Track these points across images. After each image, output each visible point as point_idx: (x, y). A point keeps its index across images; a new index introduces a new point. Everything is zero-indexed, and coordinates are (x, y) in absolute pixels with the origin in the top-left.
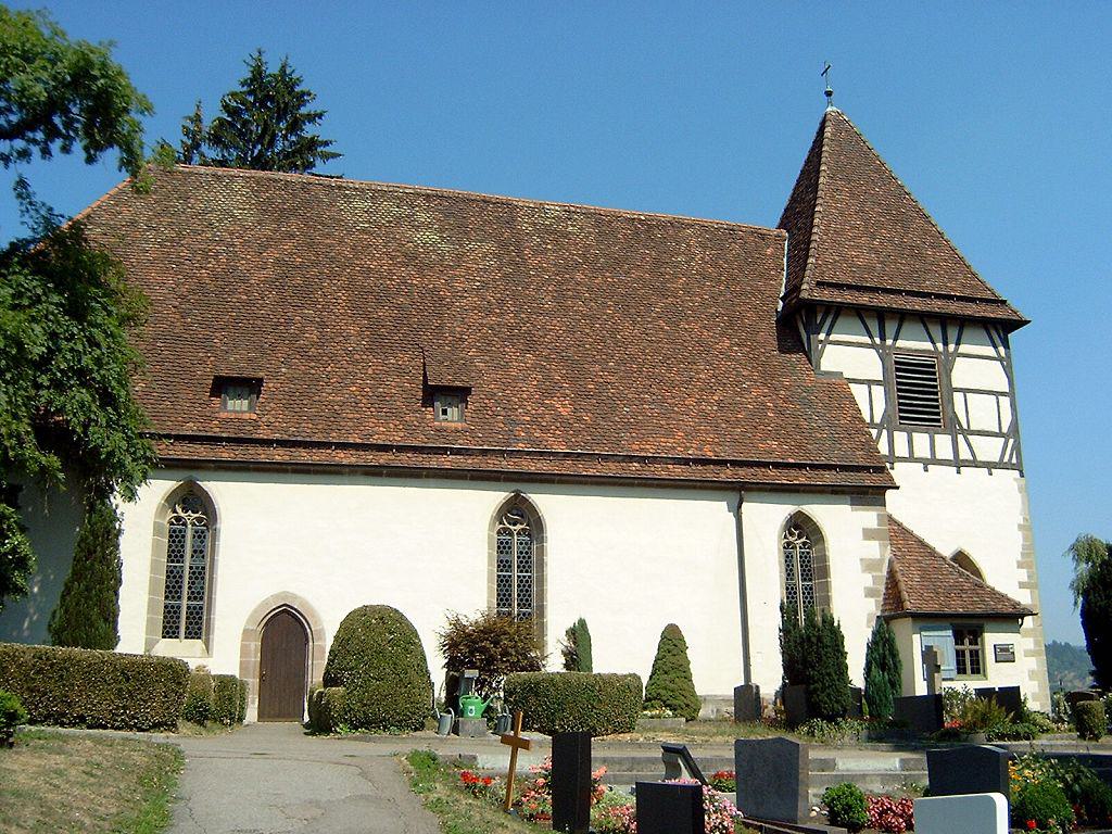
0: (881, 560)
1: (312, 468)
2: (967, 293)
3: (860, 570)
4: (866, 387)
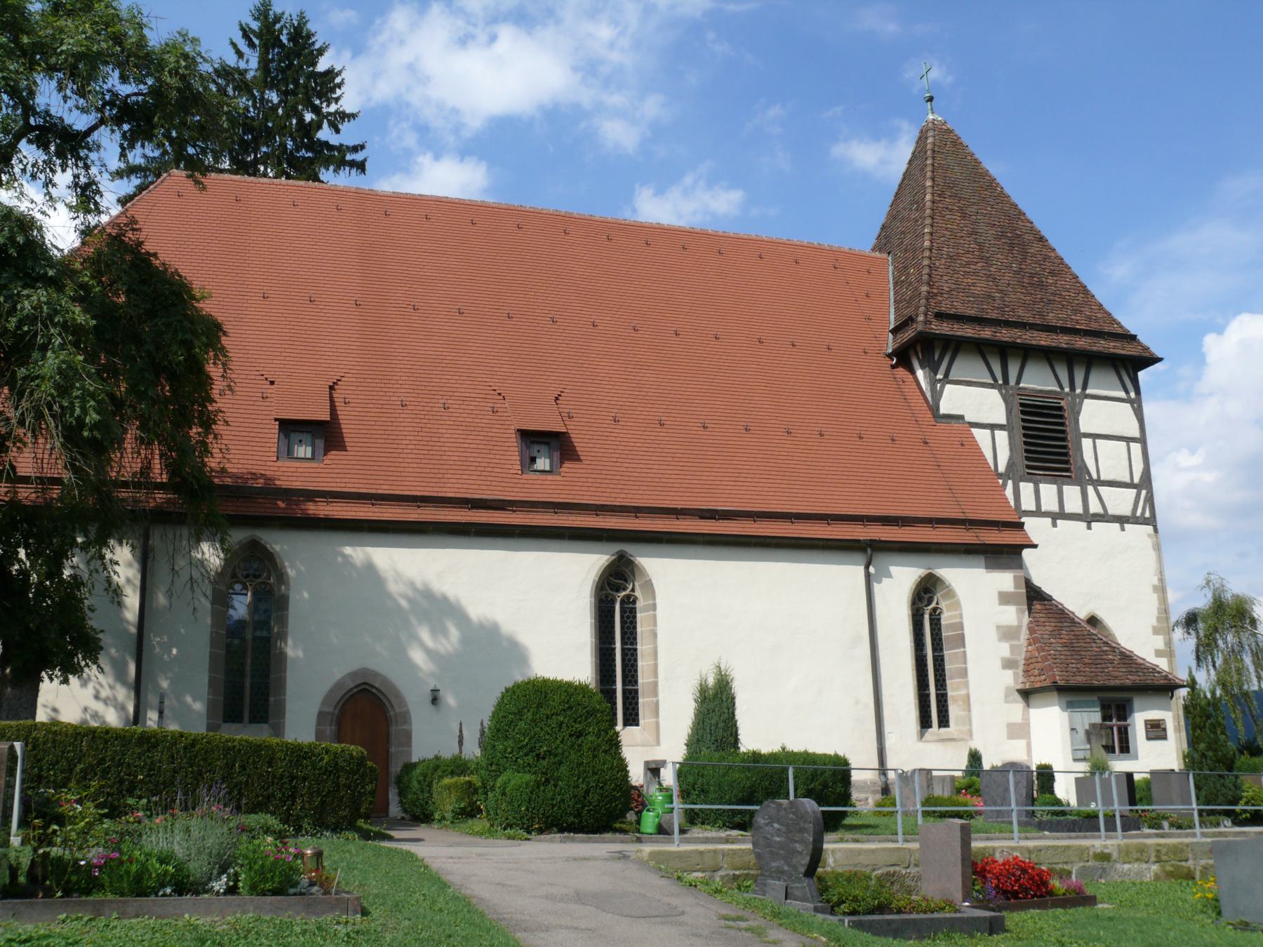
0: (1019, 627)
1: (753, 541)
2: (1094, 326)
3: (996, 639)
4: (1124, 444)
